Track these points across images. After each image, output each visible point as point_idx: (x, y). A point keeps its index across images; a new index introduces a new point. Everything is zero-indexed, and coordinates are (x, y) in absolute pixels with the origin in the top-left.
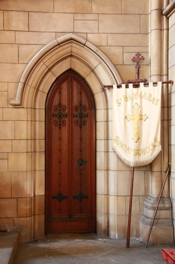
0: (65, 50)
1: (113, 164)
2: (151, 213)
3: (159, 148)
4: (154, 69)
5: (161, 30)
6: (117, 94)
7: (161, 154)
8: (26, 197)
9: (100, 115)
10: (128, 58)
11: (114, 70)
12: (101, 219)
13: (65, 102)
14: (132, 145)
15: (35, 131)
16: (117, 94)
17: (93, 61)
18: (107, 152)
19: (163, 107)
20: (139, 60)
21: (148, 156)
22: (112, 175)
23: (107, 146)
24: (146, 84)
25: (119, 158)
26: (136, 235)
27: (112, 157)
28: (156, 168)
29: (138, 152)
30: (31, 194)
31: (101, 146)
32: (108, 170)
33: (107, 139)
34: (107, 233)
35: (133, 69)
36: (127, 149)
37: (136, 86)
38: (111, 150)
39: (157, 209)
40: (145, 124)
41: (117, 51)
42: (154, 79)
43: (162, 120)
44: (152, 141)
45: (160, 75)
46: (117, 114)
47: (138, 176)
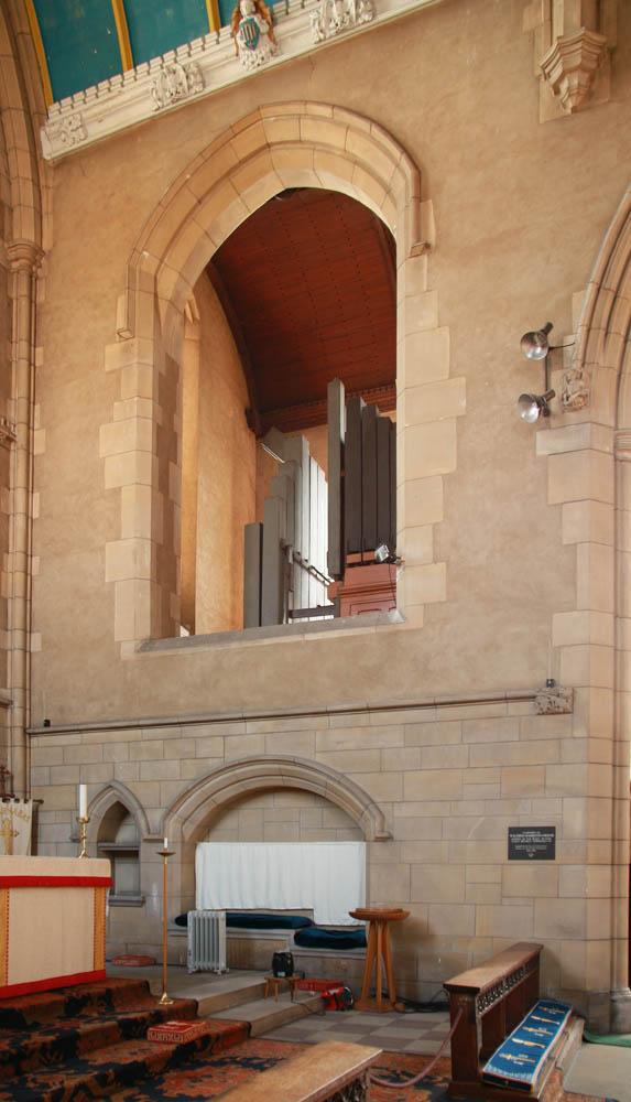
5: (25, 747)
24: (17, 801)
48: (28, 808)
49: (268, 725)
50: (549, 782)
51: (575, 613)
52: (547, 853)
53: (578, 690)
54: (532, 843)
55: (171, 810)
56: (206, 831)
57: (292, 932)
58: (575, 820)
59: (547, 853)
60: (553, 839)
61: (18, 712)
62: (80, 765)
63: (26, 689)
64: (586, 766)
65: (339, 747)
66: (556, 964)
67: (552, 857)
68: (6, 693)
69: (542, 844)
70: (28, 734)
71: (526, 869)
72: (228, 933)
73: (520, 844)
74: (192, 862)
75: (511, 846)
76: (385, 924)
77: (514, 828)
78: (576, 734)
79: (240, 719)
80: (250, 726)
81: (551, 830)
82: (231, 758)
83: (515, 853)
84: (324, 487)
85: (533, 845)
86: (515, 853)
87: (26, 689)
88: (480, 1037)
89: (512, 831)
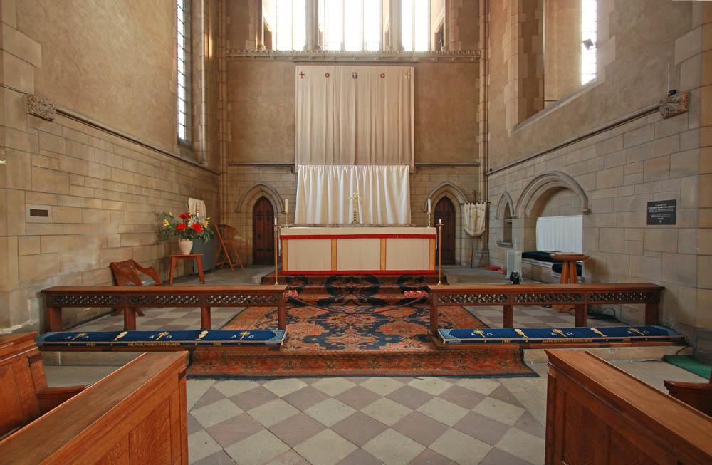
0: (445, 189)
1: (464, 235)
2: (480, 255)
3: (484, 229)
4: (482, 196)
5: (485, 181)
6: (466, 207)
7: (485, 231)
8: (697, 288)
9: (458, 215)
10: (471, 192)
11: (461, 218)
12: (458, 258)
13: (442, 210)
14: (473, 227)
15: (349, 119)
16: (466, 207)
17: (455, 193)
18: (461, 231)
19: (486, 212)
20: (475, 193)
21: (480, 232)
22: (463, 241)
23: (461, 228)
24: (479, 203)
25: (467, 233)
26: (467, 263)
27: (464, 234)
28: (482, 237)
29: (475, 231)
30: (292, 223)
31: (458, 228)
32: (461, 238)
33: (461, 225)
34: (460, 264)
35: (472, 196)
36: (470, 229)
37: (475, 204)
38: (463, 230)
39: (483, 253)
40: (479, 219)
41: (466, 189)
42: (482, 201)
43: (486, 218)
44: (481, 226)
45: (484, 200)
46: (466, 215)
47: (475, 240)
48: (484, 206)
49: (546, 156)
50: (672, 167)
51: (691, 33)
52: (671, 220)
53: (692, 92)
54: (661, 213)
55: (519, 203)
56: (539, 211)
57: (552, 264)
58: (687, 192)
59: (671, 220)
60: (675, 209)
61: (481, 168)
62: (587, 160)
63: (486, 158)
64: (699, 150)
65: (571, 162)
66: (675, 303)
67: (674, 223)
68: (478, 160)
69: (667, 213)
70: (485, 176)
71: (658, 231)
72: (570, 283)
73: (654, 213)
74: (534, 227)
75: (649, 214)
76: (569, 262)
77: (651, 202)
78: (691, 127)
79: (606, 129)
80: (542, 158)
81: (673, 202)
82: (537, 175)
83: (651, 221)
84: (327, 298)
85: (663, 214)
86: (651, 221)
87: (486, 158)
88: (203, 80)
89: (650, 204)
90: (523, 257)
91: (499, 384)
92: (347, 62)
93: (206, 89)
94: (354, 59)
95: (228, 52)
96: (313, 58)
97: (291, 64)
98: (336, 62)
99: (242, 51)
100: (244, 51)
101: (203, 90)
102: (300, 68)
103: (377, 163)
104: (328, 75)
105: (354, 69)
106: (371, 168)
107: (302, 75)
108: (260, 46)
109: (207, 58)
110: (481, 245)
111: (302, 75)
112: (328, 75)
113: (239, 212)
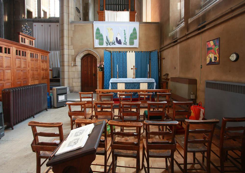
19: (145, 171)
64: (8, 140)
90: (59, 21)
91: (68, 105)
92: (47, 22)
93: (5, 30)
94: (49, 21)
95: (14, 19)
96: (38, 21)
97: (32, 22)
98: (45, 22)
99: (18, 19)
100: (19, 19)
101: (4, 30)
102: (34, 24)
103: (56, 50)
104: (42, 26)
105: (49, 24)
106: (54, 52)
107: (35, 25)
108: (24, 17)
109: (5, 22)
110: (138, 84)
111: (35, 25)
112: (42, 26)
113: (76, 66)
